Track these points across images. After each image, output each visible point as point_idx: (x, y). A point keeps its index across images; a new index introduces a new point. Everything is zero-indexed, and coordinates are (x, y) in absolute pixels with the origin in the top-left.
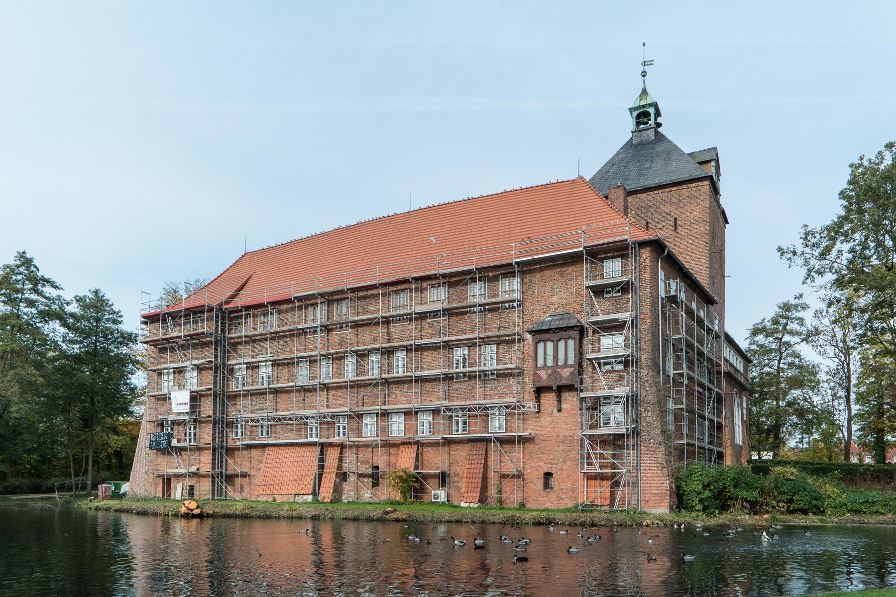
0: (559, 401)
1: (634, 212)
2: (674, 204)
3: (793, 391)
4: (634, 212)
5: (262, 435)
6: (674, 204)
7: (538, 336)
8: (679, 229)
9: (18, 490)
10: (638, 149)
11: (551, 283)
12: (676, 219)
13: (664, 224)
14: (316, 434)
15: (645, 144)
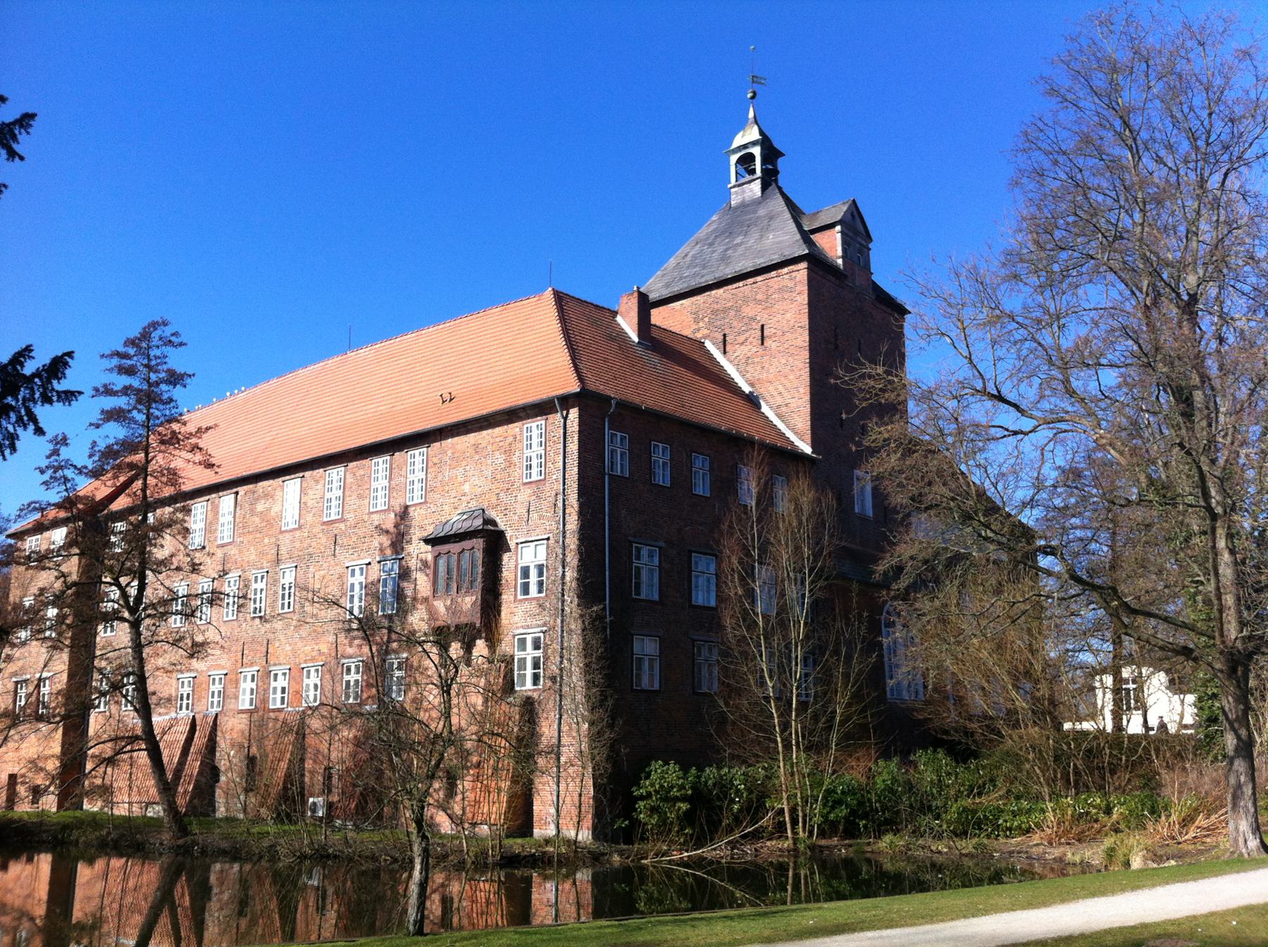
7: (444, 548)
11: (464, 463)
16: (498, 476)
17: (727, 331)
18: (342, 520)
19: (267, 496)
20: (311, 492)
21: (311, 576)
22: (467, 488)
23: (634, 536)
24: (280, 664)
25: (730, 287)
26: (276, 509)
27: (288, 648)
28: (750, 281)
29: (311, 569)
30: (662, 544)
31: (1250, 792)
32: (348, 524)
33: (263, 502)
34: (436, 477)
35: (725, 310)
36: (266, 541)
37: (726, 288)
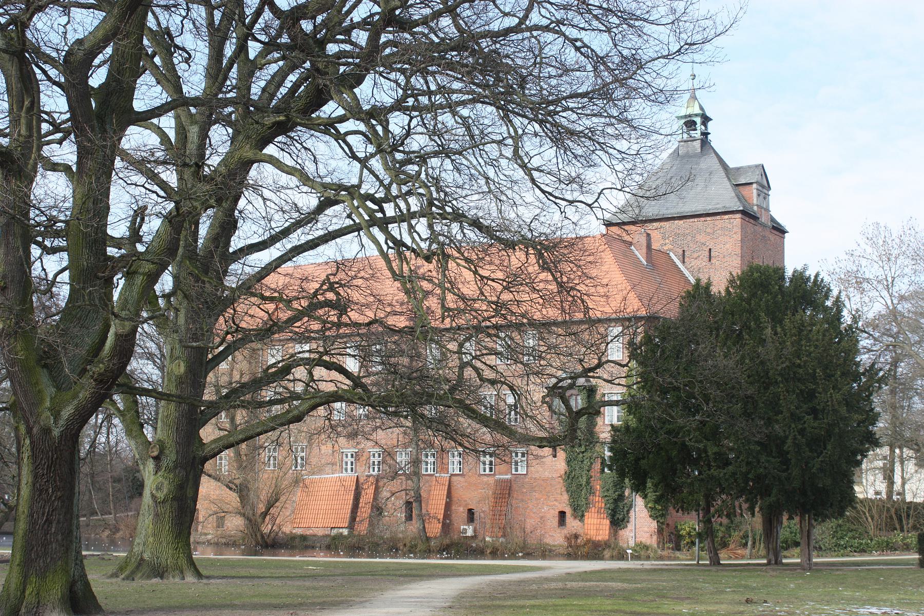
0: (524, 540)
1: (671, 239)
2: (709, 234)
6: (709, 234)
8: (713, 261)
10: (684, 161)
12: (710, 249)
15: (691, 157)
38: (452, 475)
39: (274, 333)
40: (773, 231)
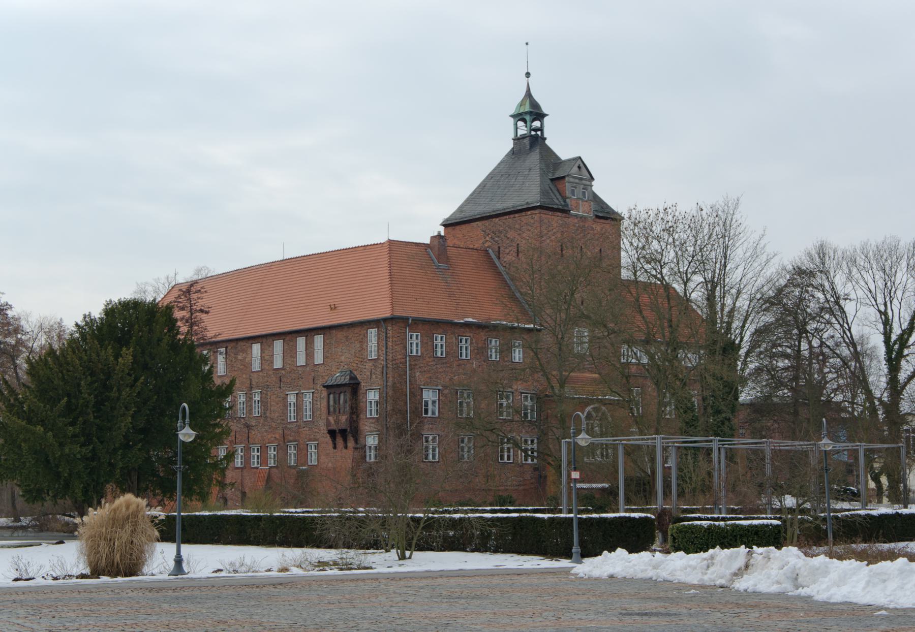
3: (740, 353)
4: (490, 236)
5: (371, 415)
7: (332, 390)
8: (520, 255)
9: (906, 336)
11: (341, 345)
12: (518, 244)
13: (510, 249)
14: (258, 462)
16: (357, 355)
17: (500, 245)
18: (283, 369)
19: (243, 351)
20: (266, 352)
21: (269, 397)
22: (343, 358)
23: (424, 385)
24: (256, 444)
25: (502, 218)
26: (248, 359)
27: (259, 435)
28: (512, 216)
29: (269, 394)
30: (440, 387)
31: (845, 507)
32: (286, 371)
33: (241, 354)
34: (328, 351)
35: (500, 232)
36: (244, 376)
37: (500, 218)
38: (271, 467)
39: (908, 340)
40: (598, 220)
